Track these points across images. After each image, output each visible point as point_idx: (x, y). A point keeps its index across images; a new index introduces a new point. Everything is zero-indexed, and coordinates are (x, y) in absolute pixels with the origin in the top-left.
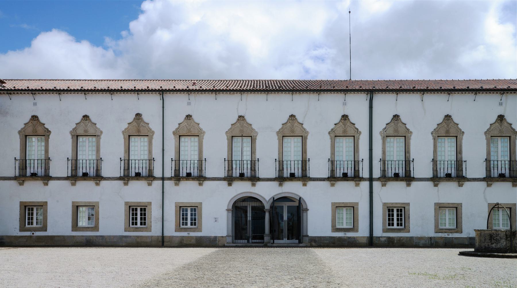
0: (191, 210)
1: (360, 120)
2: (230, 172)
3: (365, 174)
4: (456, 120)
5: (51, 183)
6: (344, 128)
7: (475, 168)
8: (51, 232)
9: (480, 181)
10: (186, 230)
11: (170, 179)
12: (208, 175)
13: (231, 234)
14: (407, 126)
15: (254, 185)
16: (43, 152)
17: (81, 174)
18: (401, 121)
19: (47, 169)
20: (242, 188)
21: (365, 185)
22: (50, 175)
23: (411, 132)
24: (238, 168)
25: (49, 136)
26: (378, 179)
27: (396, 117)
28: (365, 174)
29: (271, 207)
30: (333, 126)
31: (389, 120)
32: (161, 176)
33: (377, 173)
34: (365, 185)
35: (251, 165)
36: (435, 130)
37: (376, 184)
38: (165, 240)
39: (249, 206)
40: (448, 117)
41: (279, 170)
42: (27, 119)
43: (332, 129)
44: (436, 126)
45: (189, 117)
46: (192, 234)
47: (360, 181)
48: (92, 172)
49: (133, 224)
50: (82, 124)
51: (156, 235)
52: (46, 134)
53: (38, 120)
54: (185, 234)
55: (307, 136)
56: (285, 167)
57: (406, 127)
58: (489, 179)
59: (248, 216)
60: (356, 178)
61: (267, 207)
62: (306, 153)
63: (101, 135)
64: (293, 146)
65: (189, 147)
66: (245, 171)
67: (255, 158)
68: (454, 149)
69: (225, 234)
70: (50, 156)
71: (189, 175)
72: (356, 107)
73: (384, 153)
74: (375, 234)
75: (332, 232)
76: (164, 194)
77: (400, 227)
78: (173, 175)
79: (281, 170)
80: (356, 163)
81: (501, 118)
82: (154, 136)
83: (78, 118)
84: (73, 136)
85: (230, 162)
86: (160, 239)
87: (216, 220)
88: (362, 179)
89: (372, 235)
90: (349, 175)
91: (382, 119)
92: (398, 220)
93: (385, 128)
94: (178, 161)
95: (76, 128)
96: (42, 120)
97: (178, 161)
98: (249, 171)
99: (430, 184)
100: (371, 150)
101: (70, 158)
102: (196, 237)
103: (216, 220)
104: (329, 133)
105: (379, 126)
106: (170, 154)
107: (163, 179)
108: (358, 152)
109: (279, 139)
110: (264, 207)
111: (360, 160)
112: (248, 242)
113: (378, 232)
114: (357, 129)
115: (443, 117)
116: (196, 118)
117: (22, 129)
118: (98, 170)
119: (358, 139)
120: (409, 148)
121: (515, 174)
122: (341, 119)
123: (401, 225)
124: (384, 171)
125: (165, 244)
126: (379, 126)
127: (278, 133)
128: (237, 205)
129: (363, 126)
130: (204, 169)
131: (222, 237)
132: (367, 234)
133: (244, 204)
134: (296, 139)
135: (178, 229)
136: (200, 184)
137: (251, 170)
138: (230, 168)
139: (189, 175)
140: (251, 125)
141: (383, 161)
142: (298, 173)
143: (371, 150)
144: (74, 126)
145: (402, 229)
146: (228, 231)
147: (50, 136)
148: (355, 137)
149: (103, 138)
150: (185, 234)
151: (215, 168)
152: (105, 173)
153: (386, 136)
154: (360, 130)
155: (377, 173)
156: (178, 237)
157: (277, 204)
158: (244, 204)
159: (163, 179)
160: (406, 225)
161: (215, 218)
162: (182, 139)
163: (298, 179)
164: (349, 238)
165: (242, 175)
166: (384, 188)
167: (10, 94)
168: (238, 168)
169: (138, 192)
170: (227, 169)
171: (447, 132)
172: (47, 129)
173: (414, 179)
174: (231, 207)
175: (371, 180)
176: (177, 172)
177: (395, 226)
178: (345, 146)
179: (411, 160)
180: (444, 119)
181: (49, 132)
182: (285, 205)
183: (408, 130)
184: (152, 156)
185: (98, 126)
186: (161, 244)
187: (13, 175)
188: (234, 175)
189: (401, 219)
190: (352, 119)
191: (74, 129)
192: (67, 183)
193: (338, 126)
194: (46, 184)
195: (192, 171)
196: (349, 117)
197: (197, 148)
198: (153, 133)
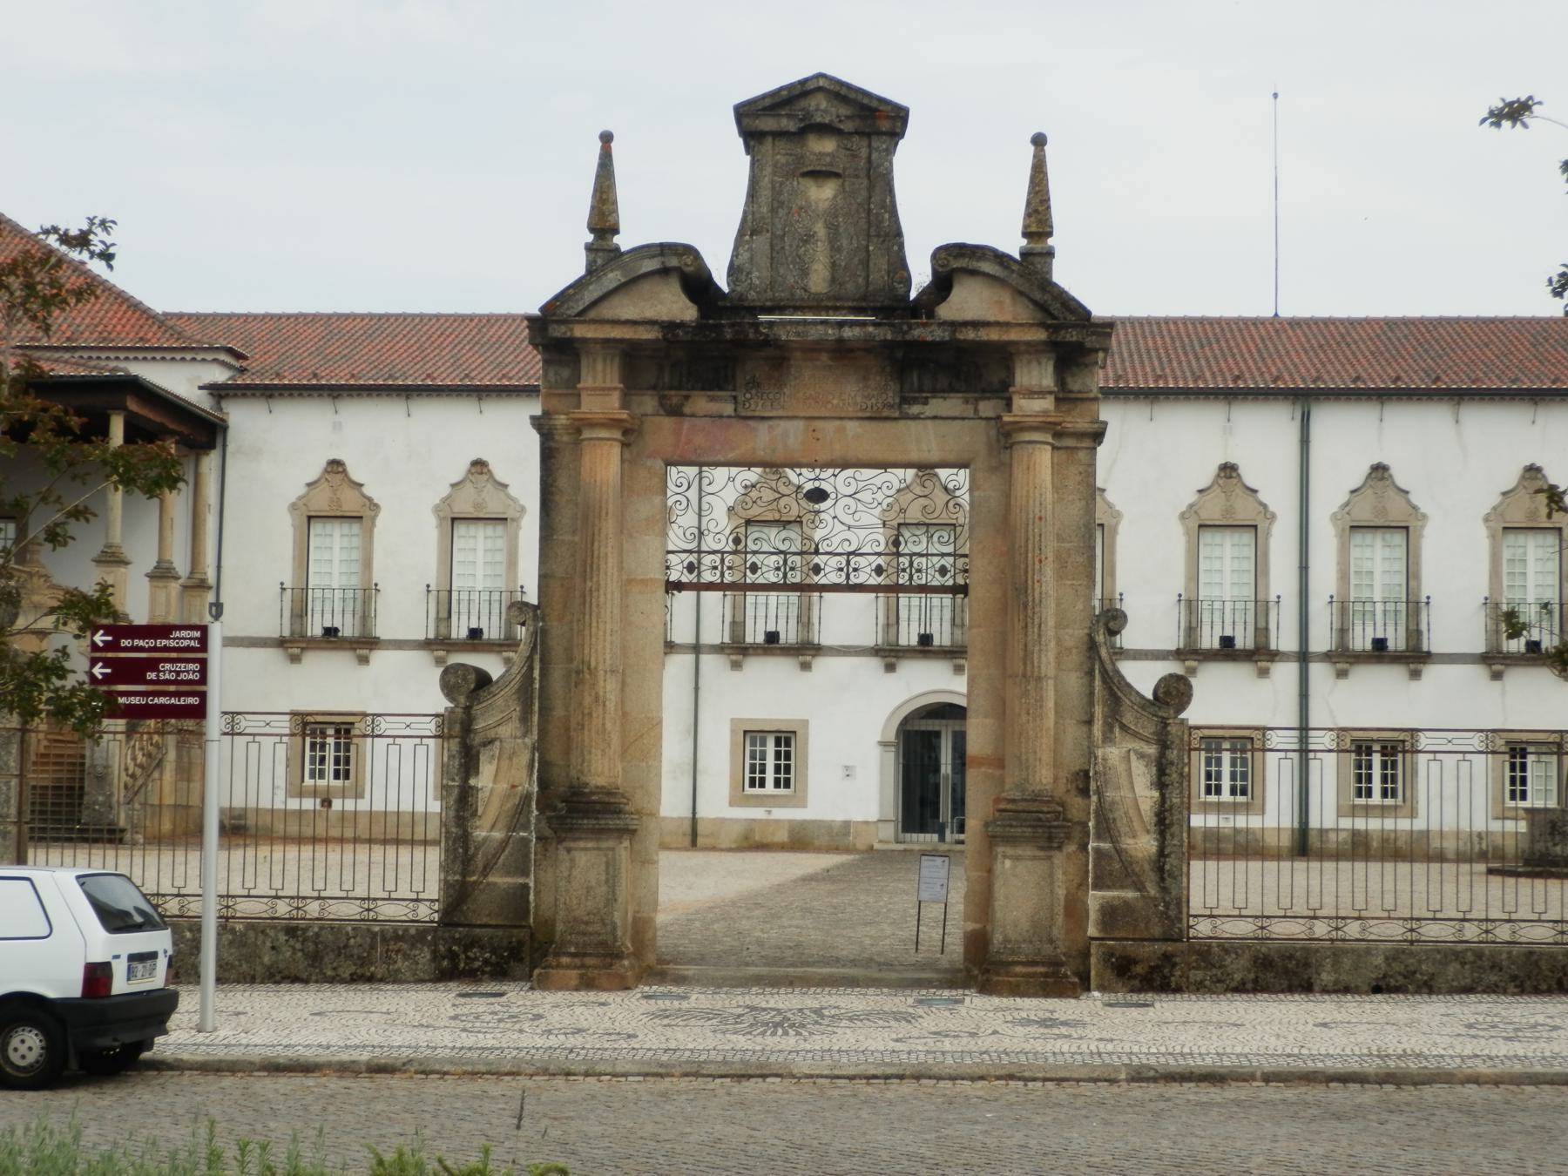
0: (778, 743)
2: (893, 630)
7: (1456, 624)
9: (1473, 662)
10: (760, 801)
12: (1436, 648)
13: (891, 815)
14: (1414, 498)
17: (317, 631)
18: (1394, 483)
19: (366, 617)
21: (1285, 673)
22: (1273, 647)
23: (1424, 516)
24: (915, 616)
25: (373, 519)
26: (1328, 657)
28: (1285, 640)
30: (1192, 497)
31: (1357, 479)
32: (691, 640)
33: (1321, 640)
34: (1285, 673)
35: (954, 610)
36: (1494, 508)
37: (1318, 671)
38: (700, 829)
41: (733, 623)
42: (314, 470)
43: (1191, 506)
44: (1496, 499)
46: (781, 814)
47: (1272, 661)
49: (752, 784)
50: (468, 485)
51: (675, 815)
54: (758, 813)
55: (1117, 524)
57: (1409, 502)
58: (1494, 661)
59: (943, 760)
62: (1418, 577)
63: (521, 517)
65: (333, 553)
66: (935, 630)
67: (1418, 594)
68: (1401, 566)
69: (873, 817)
70: (377, 577)
72: (1260, 440)
73: (1344, 576)
74: (1314, 823)
75: (731, 804)
76: (701, 693)
77: (1389, 801)
78: (727, 640)
79: (300, 613)
83: (459, 470)
84: (441, 519)
85: (1191, 605)
86: (687, 826)
87: (848, 772)
88: (1274, 656)
89: (1307, 823)
90: (1239, 644)
92: (1384, 779)
93: (1347, 504)
95: (449, 496)
96: (356, 474)
98: (947, 626)
99: (1478, 672)
100: (1304, 569)
101: (288, 585)
102: (790, 821)
103: (848, 772)
104: (1486, 519)
105: (1328, 498)
107: (697, 649)
108: (1267, 574)
109: (1187, 533)
111: (1273, 598)
112: (942, 839)
113: (1325, 815)
114: (1265, 506)
115: (1366, 469)
117: (300, 498)
118: (1414, 634)
119: (1268, 534)
120: (1418, 564)
122: (1218, 476)
123: (1394, 795)
125: (700, 841)
126: (1328, 498)
128: (909, 728)
129: (1278, 494)
130: (815, 620)
131: (867, 823)
132: (1288, 821)
135: (738, 800)
136: (806, 666)
137: (953, 624)
138: (893, 620)
140: (1256, 491)
141: (1343, 607)
143: (1304, 569)
144: (445, 491)
145: (1396, 807)
146: (881, 805)
147: (379, 521)
148: (1254, 529)
150: (758, 813)
152: (1436, 641)
154: (1272, 508)
155: (1321, 640)
156: (736, 821)
159: (697, 649)
160: (1408, 794)
161: (847, 768)
163: (1397, 658)
166: (1342, 682)
167: (271, 396)
168: (915, 616)
170: (432, 615)
172: (370, 499)
173: (818, 650)
174: (891, 737)
175: (1304, 657)
177: (1376, 798)
178: (1226, 561)
179: (1273, 598)
180: (1523, 477)
181: (374, 507)
183: (1415, 508)
184: (370, 579)
185: (512, 491)
186: (687, 841)
188: (749, 639)
189: (1394, 777)
190: (1249, 477)
191: (444, 500)
193: (1208, 497)
194: (364, 660)
195: (484, 626)
196: (1241, 471)
198: (1272, 517)
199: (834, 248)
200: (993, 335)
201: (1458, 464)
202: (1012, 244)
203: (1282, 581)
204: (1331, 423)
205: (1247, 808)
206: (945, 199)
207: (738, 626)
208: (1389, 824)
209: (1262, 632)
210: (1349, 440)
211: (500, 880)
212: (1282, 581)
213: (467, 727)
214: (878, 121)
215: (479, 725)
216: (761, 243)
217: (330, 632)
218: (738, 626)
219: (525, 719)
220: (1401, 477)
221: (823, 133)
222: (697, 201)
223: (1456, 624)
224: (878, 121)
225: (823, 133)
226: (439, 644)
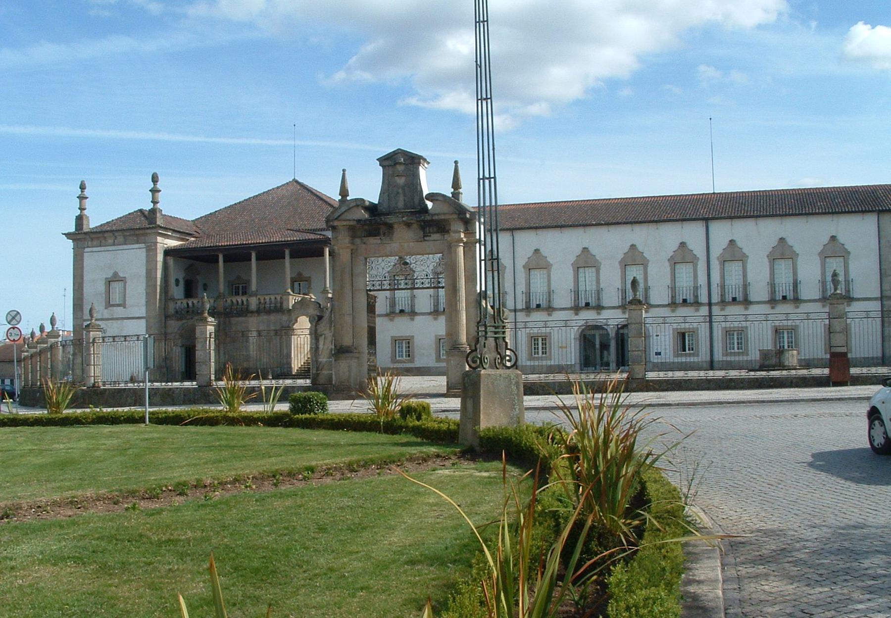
1: (697, 245)
3: (704, 299)
4: (691, 247)
5: (417, 318)
6: (682, 255)
8: (418, 363)
10: (538, 359)
11: (521, 310)
12: (604, 305)
13: (578, 361)
15: (599, 314)
16: (594, 283)
17: (397, 311)
20: (588, 316)
27: (732, 242)
28: (704, 299)
29: (617, 333)
30: (672, 254)
33: (715, 298)
34: (704, 311)
39: (597, 333)
40: (782, 240)
45: (537, 251)
46: (544, 363)
48: (407, 309)
52: (742, 259)
53: (588, 251)
56: (777, 289)
60: (697, 304)
61: (612, 334)
64: (734, 269)
65: (588, 277)
71: (538, 306)
72: (692, 234)
73: (528, 285)
80: (696, 288)
81: (833, 238)
82: (699, 263)
85: (577, 293)
91: (719, 245)
94: (528, 294)
97: (528, 294)
105: (717, 251)
106: (521, 287)
110: (608, 334)
116: (544, 252)
118: (746, 295)
121: (888, 293)
124: (723, 295)
126: (717, 251)
127: (620, 262)
133: (593, 332)
134: (838, 259)
135: (531, 358)
139: (685, 301)
141: (723, 287)
142: (790, 296)
149: (800, 262)
150: (684, 359)
151: (563, 299)
152: (753, 297)
153: (723, 262)
155: (715, 298)
157: (621, 331)
158: (593, 332)
162: (532, 272)
164: (216, 371)
165: (587, 304)
169: (694, 318)
171: (782, 254)
173: (751, 303)
175: (710, 304)
176: (528, 303)
180: (729, 245)
182: (597, 333)
187: (569, 306)
192: (430, 317)
197: (546, 280)
199: (405, 195)
200: (442, 217)
201: (859, 233)
202: (448, 191)
203: (702, 280)
204: (715, 226)
205: (693, 355)
206: (432, 181)
207: (393, 304)
208: (741, 358)
209: (696, 297)
210: (722, 232)
211: (325, 372)
212: (508, 286)
213: (316, 330)
214: (414, 161)
215: (319, 331)
216: (386, 198)
217: (402, 311)
218: (393, 304)
219: (330, 327)
220: (740, 243)
221: (401, 166)
222: (368, 187)
223: (759, 292)
224: (414, 161)
225: (401, 166)
226: (824, 299)
